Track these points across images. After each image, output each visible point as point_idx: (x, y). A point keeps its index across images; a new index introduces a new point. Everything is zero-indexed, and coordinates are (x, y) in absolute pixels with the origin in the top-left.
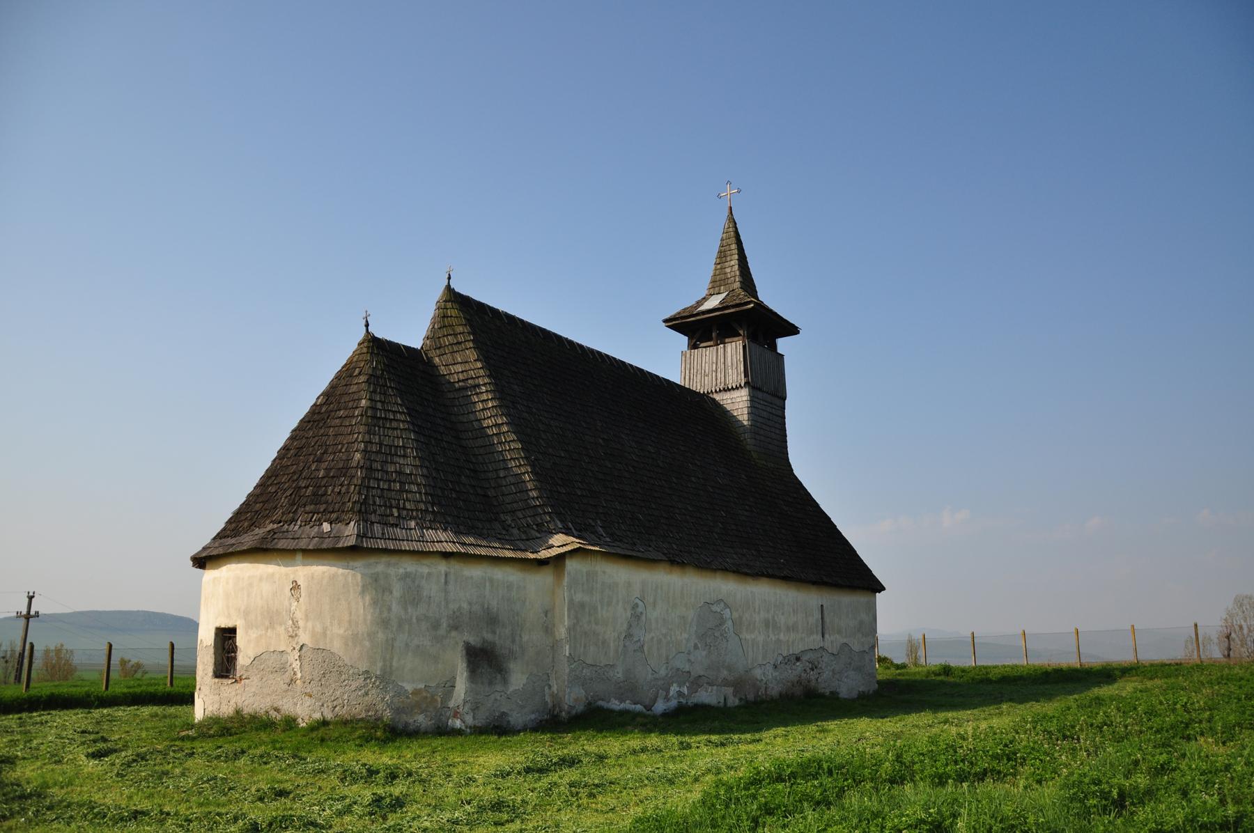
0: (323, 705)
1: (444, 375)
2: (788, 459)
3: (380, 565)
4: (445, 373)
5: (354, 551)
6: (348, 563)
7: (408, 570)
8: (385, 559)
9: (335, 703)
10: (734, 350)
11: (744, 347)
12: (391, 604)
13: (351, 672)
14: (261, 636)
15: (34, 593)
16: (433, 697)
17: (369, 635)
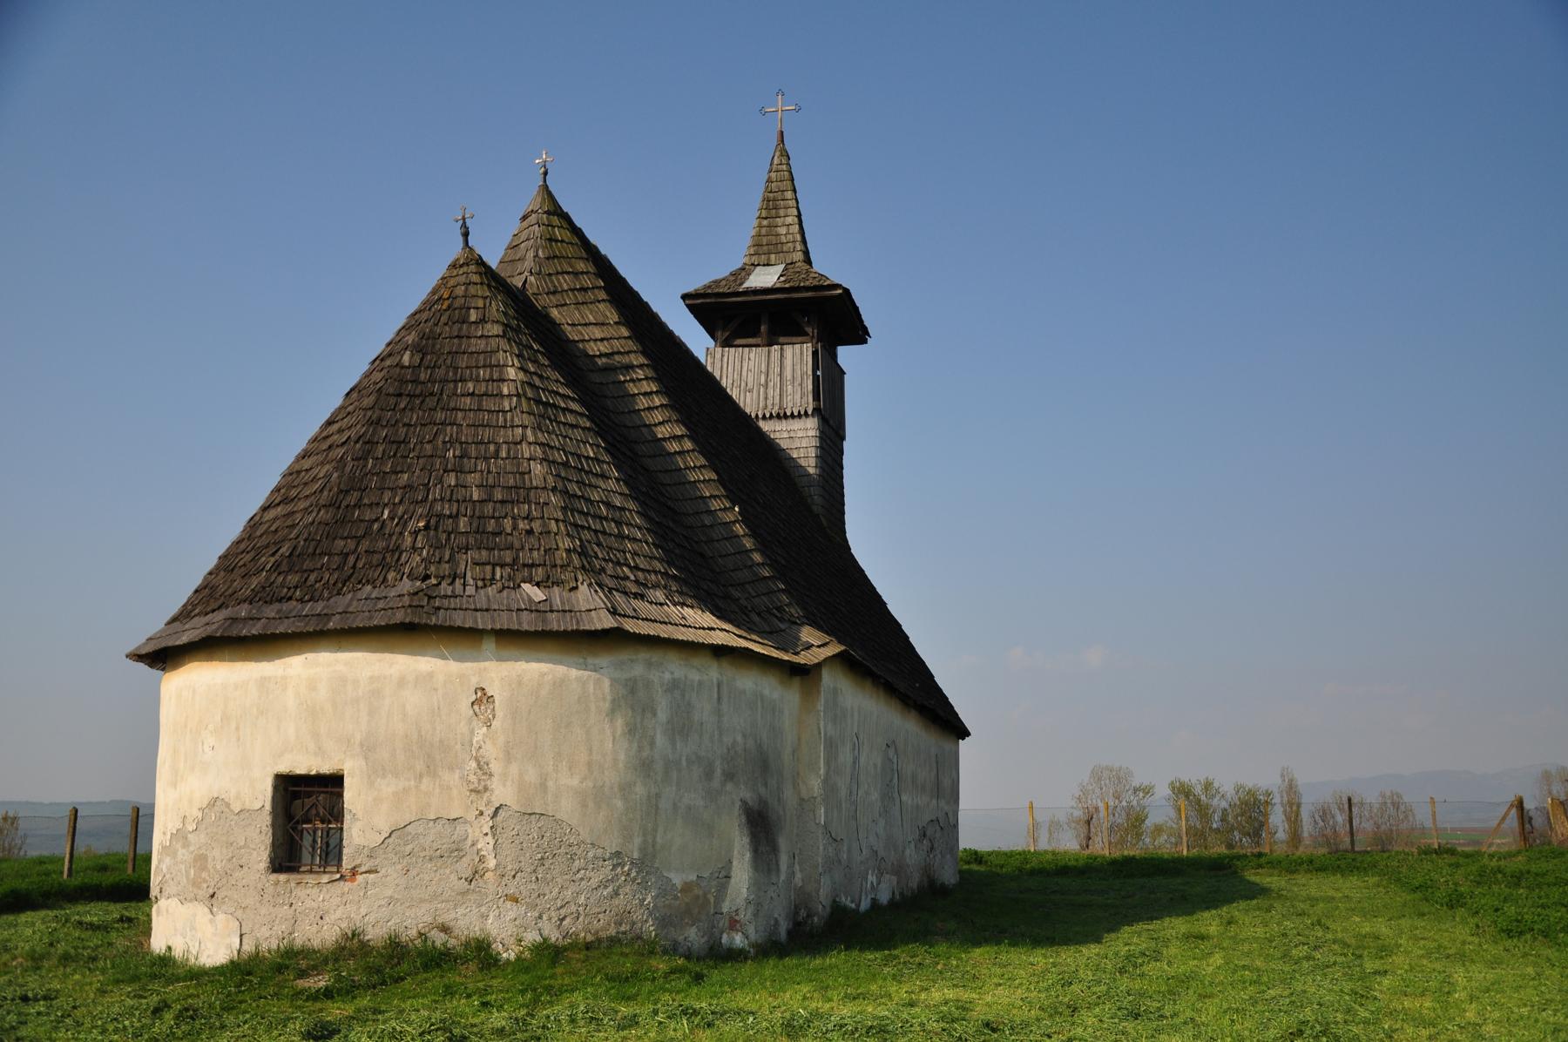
0: (540, 917)
1: (574, 341)
2: (844, 532)
4: (577, 339)
6: (585, 659)
7: (677, 675)
8: (643, 655)
9: (563, 912)
10: (797, 357)
11: (815, 354)
12: (655, 734)
13: (591, 855)
14: (406, 790)
16: (705, 895)
17: (622, 789)
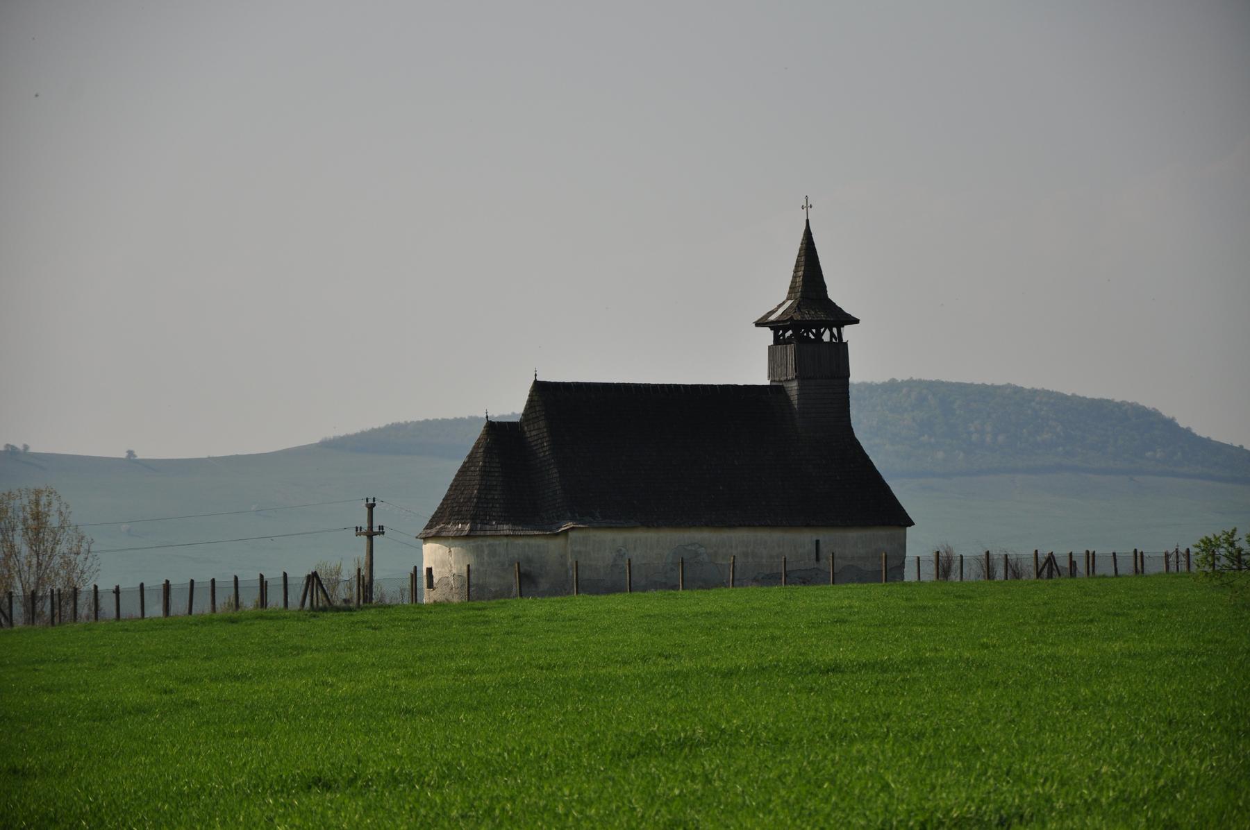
3: (479, 542)
5: (468, 536)
15: (374, 500)
